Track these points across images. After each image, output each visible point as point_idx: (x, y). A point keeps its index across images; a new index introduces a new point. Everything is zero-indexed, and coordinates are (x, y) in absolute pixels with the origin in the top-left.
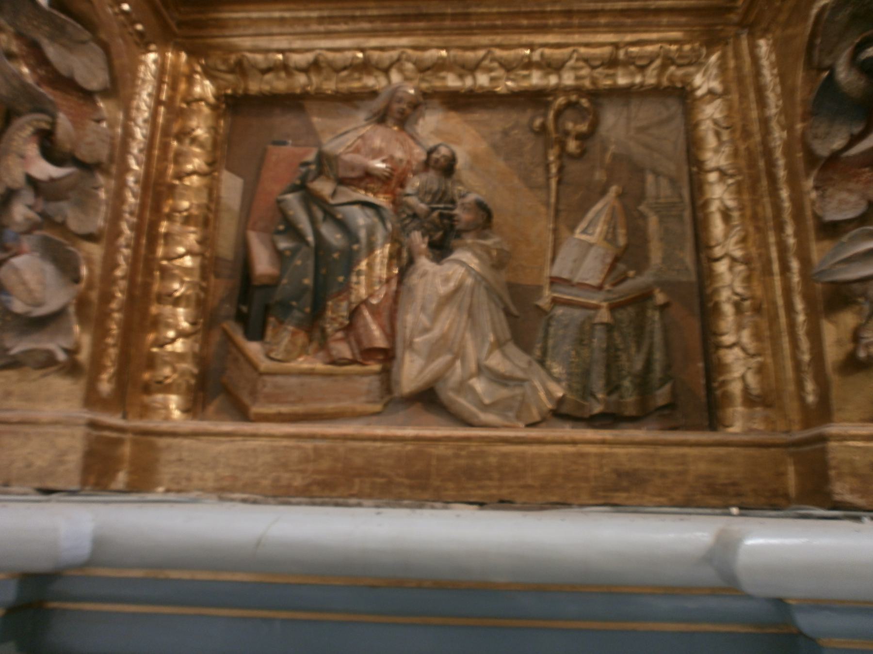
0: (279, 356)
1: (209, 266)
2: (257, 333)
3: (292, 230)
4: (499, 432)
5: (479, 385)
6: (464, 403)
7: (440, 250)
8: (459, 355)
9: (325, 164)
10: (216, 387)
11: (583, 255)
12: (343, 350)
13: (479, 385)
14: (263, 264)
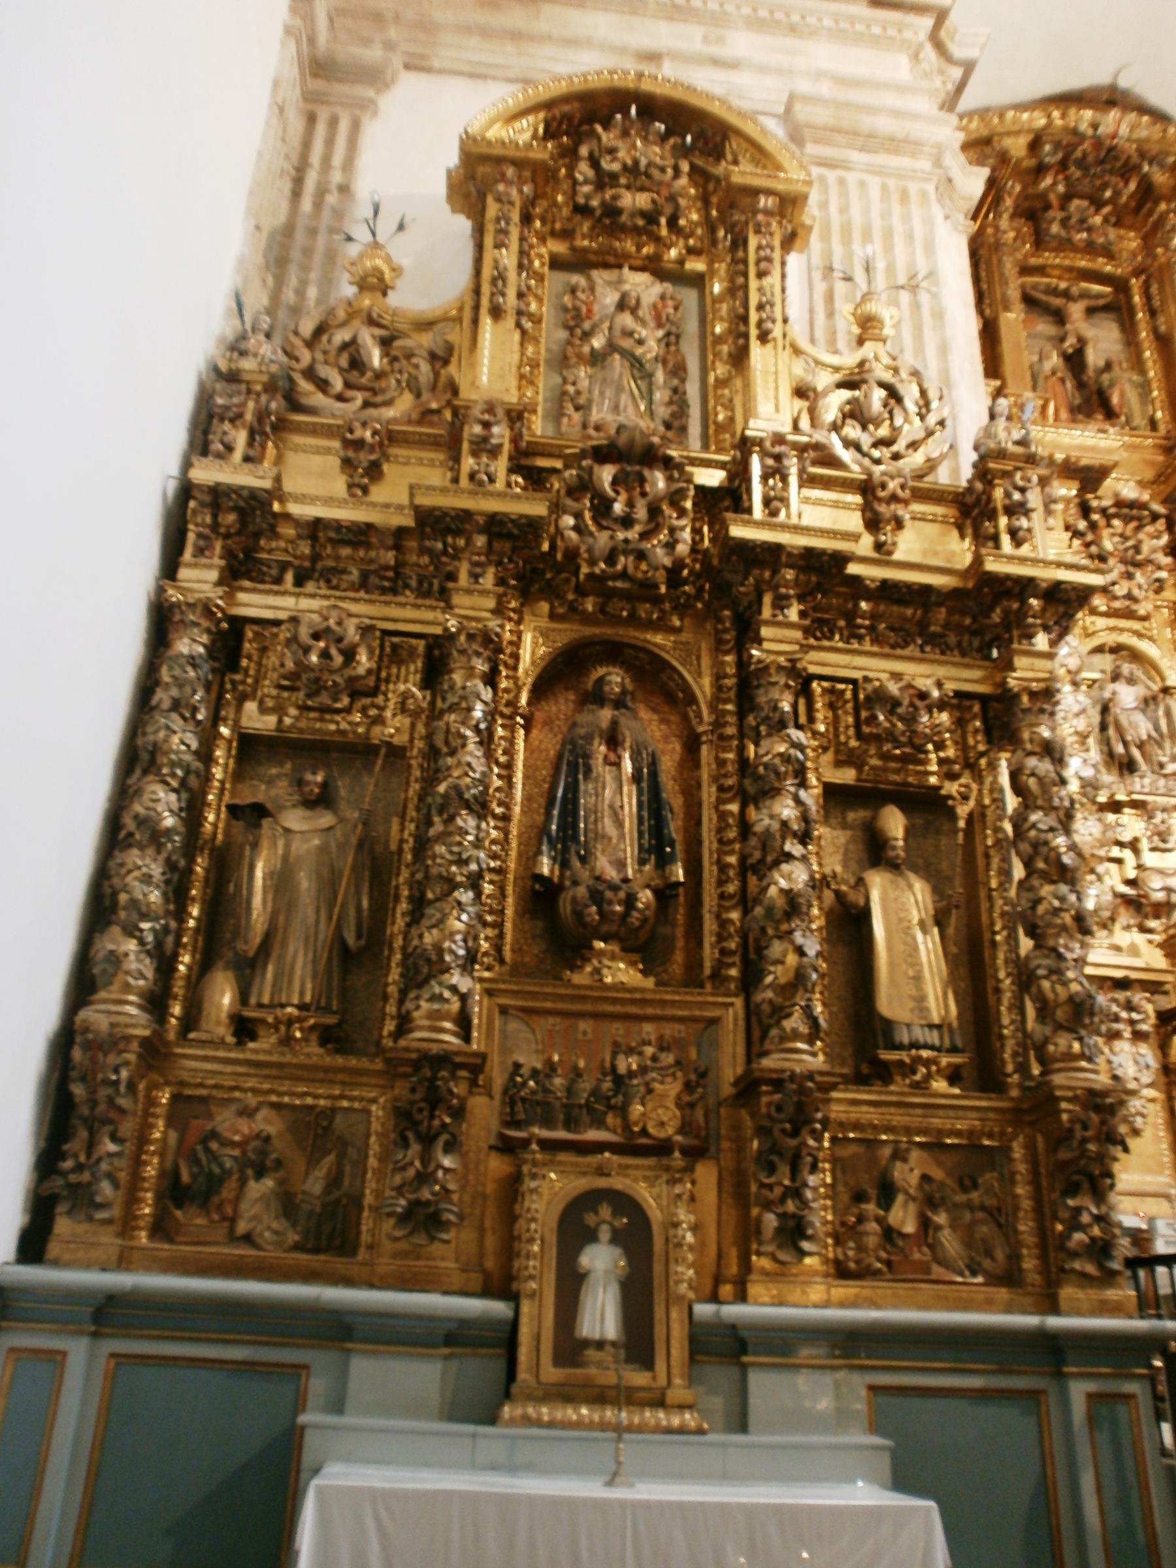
0: (191, 1218)
1: (162, 1174)
2: (179, 1206)
3: (197, 1161)
4: (272, 1253)
5: (267, 1234)
6: (260, 1241)
7: (260, 1174)
8: (260, 1221)
9: (214, 1135)
10: (161, 1228)
11: (315, 1184)
12: (216, 1217)
13: (267, 1234)
14: (185, 1177)
